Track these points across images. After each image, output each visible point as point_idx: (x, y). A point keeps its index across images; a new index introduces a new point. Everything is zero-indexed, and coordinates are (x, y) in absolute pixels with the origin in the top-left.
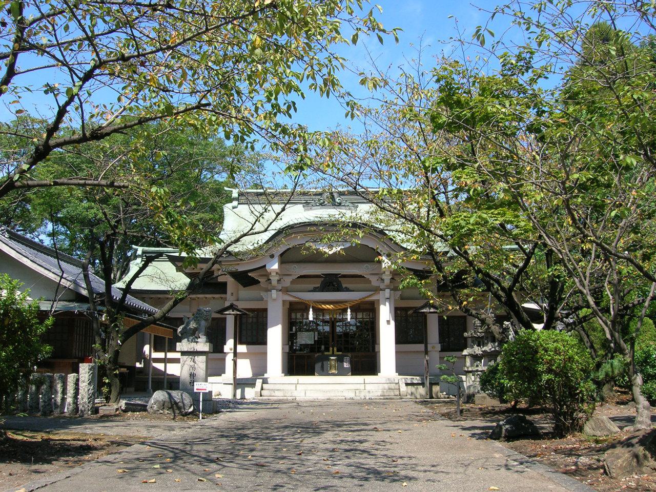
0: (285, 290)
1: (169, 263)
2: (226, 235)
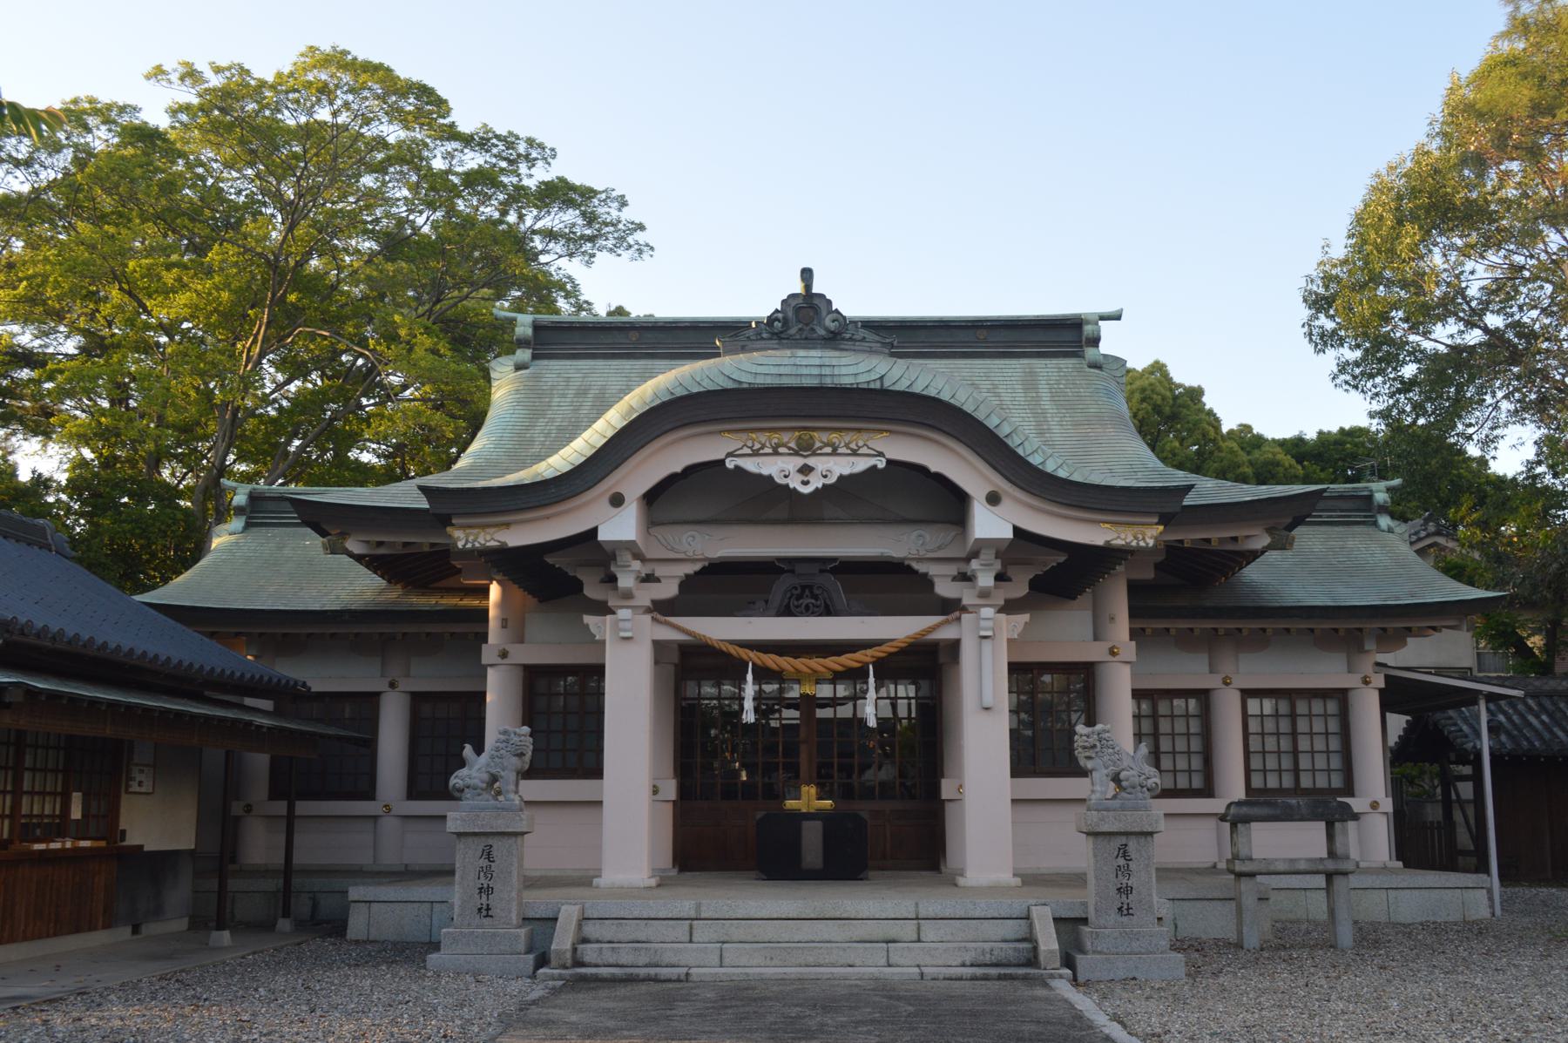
0: (663, 608)
2: (480, 460)
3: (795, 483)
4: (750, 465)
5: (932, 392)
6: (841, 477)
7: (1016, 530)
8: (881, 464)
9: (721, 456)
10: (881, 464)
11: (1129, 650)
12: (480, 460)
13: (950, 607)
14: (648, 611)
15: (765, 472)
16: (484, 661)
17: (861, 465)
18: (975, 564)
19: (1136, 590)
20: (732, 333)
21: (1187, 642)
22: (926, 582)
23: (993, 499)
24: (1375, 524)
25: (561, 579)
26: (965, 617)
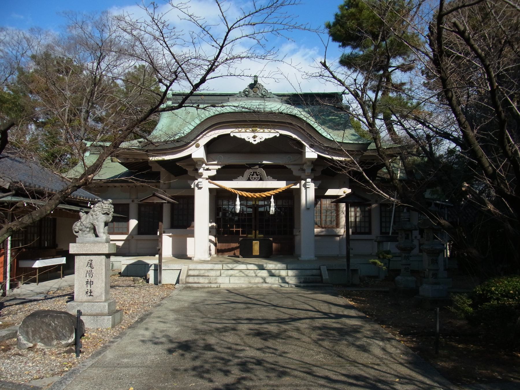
3: (251, 140)
4: (238, 135)
6: (266, 139)
10: (278, 135)
14: (207, 179)
22: (290, 171)
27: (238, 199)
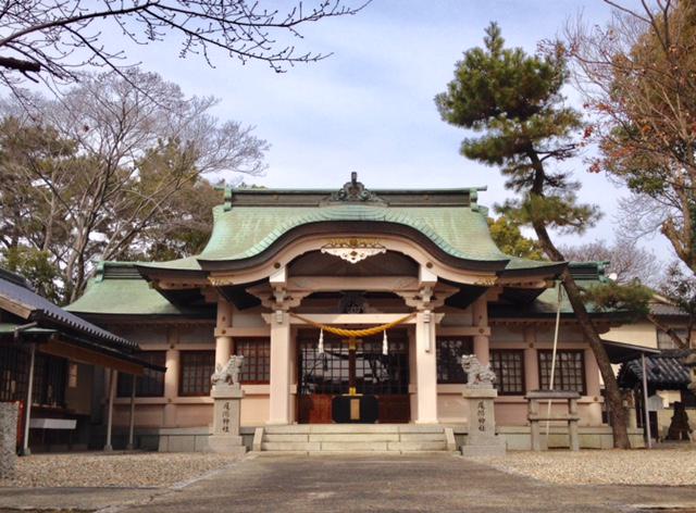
0: (293, 311)
1: (144, 282)
2: (214, 249)
3: (349, 259)
4: (331, 252)
5: (405, 222)
6: (368, 257)
7: (439, 278)
8: (384, 251)
9: (319, 248)
10: (384, 251)
11: (488, 331)
12: (214, 249)
13: (412, 310)
14: (288, 311)
15: (337, 254)
16: (216, 335)
17: (376, 252)
18: (422, 292)
19: (491, 307)
20: (324, 196)
21: (513, 329)
22: (402, 300)
23: (429, 266)
24: (598, 279)
25: (251, 300)
26: (418, 314)
27: (322, 335)
